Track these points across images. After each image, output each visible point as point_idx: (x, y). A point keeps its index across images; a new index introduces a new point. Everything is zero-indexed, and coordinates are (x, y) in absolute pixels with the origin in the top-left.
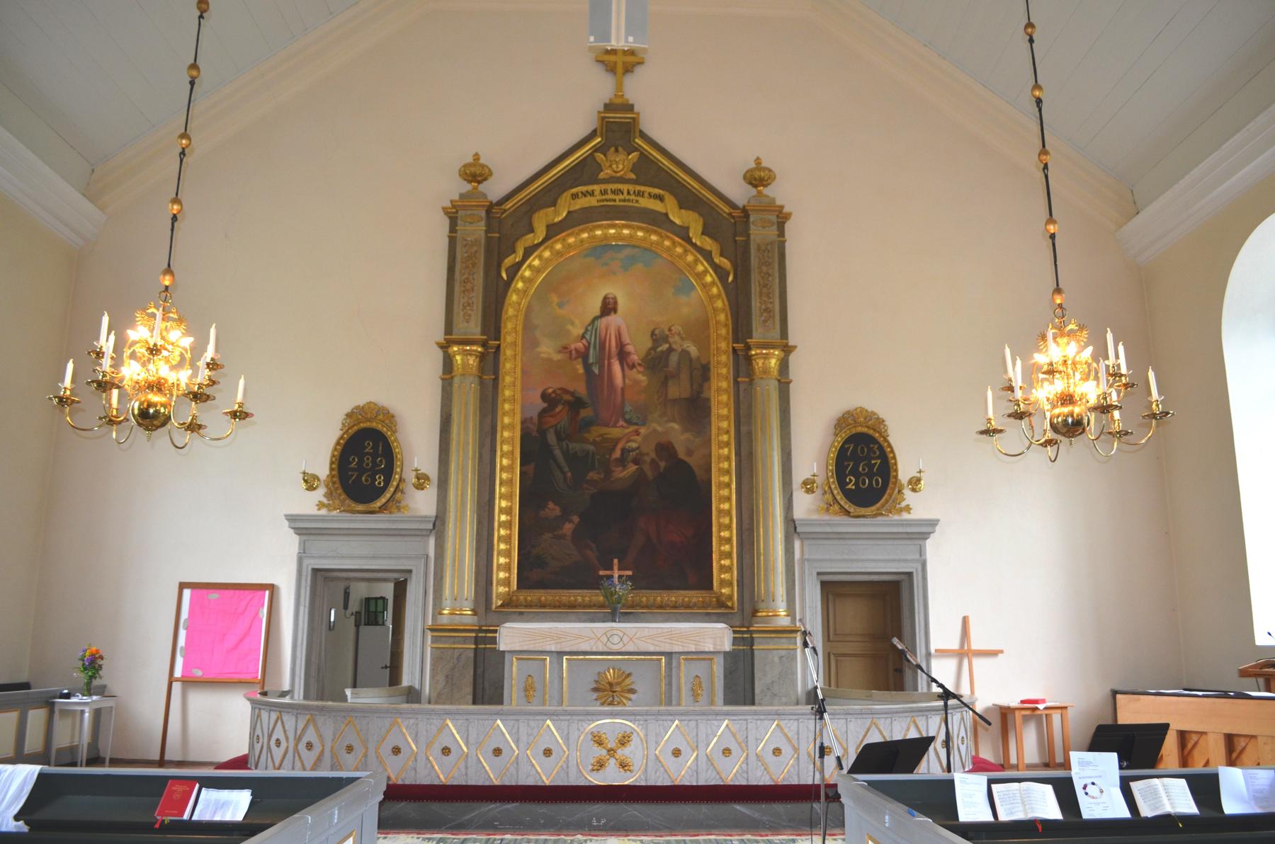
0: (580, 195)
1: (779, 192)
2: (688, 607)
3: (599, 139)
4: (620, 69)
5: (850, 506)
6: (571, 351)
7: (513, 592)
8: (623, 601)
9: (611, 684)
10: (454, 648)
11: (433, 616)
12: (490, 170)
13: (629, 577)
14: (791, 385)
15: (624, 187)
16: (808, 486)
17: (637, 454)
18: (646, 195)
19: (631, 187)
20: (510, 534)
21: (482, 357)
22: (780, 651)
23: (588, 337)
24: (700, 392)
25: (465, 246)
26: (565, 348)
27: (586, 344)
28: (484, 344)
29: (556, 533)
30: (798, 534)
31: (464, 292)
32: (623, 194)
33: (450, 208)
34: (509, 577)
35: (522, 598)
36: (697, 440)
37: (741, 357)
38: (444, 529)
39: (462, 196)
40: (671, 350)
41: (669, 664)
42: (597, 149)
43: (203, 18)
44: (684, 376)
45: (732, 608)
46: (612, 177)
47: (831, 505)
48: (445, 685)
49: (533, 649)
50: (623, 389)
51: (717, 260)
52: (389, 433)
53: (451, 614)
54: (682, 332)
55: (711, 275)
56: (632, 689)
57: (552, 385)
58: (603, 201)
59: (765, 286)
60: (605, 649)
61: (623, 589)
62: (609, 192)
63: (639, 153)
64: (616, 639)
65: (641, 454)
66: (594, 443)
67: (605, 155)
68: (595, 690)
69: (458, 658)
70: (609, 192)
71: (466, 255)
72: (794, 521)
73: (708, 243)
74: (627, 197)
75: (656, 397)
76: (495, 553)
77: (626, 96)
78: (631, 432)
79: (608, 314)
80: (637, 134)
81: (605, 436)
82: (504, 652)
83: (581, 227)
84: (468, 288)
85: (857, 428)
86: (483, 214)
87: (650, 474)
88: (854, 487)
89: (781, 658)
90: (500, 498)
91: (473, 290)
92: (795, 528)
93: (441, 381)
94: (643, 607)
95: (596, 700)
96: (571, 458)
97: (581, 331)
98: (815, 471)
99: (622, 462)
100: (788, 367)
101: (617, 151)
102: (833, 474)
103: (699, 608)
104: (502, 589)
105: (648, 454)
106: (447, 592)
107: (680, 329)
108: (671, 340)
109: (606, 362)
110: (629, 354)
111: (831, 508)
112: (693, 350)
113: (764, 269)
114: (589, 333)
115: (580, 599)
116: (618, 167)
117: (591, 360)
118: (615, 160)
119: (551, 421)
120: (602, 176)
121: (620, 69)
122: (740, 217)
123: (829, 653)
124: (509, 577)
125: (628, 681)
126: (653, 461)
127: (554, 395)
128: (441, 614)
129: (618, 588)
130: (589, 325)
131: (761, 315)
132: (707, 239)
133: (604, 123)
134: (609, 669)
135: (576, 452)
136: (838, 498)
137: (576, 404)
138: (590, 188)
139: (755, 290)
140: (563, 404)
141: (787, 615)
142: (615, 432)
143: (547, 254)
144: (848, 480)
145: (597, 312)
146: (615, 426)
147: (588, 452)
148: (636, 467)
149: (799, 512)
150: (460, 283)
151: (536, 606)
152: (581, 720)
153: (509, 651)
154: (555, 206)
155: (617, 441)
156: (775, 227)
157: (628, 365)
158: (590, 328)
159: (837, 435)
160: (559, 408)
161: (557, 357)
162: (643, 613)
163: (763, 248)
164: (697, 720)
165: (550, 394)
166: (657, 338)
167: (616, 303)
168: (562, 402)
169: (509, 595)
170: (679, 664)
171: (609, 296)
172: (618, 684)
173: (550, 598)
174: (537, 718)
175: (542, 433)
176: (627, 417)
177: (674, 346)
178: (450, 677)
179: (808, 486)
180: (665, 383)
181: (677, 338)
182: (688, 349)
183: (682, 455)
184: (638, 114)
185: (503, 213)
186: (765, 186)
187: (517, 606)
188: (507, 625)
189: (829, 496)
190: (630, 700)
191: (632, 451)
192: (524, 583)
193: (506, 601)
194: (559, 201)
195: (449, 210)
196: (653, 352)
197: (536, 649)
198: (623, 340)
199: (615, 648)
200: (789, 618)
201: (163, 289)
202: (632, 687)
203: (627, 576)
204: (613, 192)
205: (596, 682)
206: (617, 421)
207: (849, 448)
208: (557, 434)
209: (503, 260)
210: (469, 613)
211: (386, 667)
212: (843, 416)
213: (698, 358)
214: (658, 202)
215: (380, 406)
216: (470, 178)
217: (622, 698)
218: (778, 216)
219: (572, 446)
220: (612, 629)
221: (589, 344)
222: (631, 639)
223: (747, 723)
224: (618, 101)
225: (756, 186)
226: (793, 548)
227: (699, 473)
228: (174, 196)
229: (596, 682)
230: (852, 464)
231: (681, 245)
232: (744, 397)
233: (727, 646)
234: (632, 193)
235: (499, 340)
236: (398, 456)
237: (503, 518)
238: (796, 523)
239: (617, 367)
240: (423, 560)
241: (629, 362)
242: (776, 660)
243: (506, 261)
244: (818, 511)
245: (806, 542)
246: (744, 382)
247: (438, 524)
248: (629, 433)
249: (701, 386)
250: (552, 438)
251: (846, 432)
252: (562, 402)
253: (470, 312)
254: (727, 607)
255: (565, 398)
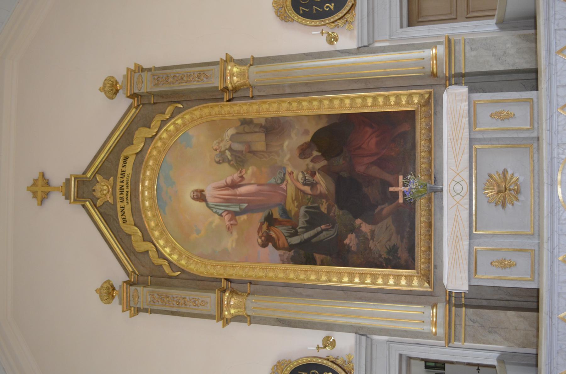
0: (123, 217)
1: (120, 74)
2: (429, 130)
3: (87, 203)
4: (46, 189)
5: (347, 6)
6: (231, 225)
7: (418, 273)
8: (425, 182)
9: (499, 192)
10: (465, 325)
11: (437, 340)
12: (105, 282)
13: (405, 177)
14: (255, 57)
15: (119, 185)
16: (332, 40)
17: (307, 173)
18: (124, 169)
19: (119, 180)
20: (370, 274)
21: (234, 292)
22: (466, 51)
23: (220, 212)
24: (261, 126)
25: (154, 302)
26: (229, 228)
27: (226, 213)
28: (224, 291)
29: (369, 238)
30: (369, 45)
31: (186, 305)
32: (123, 186)
33: (131, 312)
34: (405, 276)
35: (422, 266)
36: (296, 127)
37: (235, 95)
38: (365, 327)
39: (120, 304)
40: (230, 149)
41: (480, 141)
42: (95, 205)
44: (248, 138)
45: (430, 93)
46: (112, 194)
47: (347, 21)
48: (498, 334)
49: (467, 261)
50: (259, 185)
51: (168, 116)
52: (291, 366)
53: (436, 327)
54: (217, 141)
55: (177, 120)
56: (503, 173)
57: (256, 239)
58: (127, 200)
59: (182, 78)
60: (467, 197)
61: (413, 182)
62: (121, 196)
63: (97, 175)
64: (458, 187)
65: (307, 171)
66: (299, 207)
67: (98, 199)
68: (504, 205)
69: (474, 323)
70: (121, 196)
71: (160, 302)
72: (359, 48)
73: (156, 123)
74: (125, 183)
75: (265, 159)
76: (385, 287)
77: (62, 184)
78: (290, 178)
79: (205, 196)
80: (84, 176)
81: (294, 199)
82: (470, 286)
83: (143, 216)
84: (183, 302)
85: (288, 5)
86: (132, 288)
87: (324, 163)
88: (333, 4)
89: (472, 49)
90: (341, 282)
91: (184, 298)
92: (365, 46)
93: (252, 325)
94: (430, 167)
95: (513, 205)
96: (310, 225)
97: (217, 216)
98: (319, 32)
99: (313, 185)
100: (242, 60)
101: (94, 190)
102: (323, 21)
103: (430, 121)
104: (415, 282)
105: (307, 165)
106: (418, 328)
107: (215, 142)
108: (223, 149)
109: (239, 198)
110: (233, 181)
111: (348, 20)
112: (231, 132)
113: (170, 80)
114: (218, 211)
115: (423, 219)
116: (105, 190)
117: (237, 209)
118: (100, 191)
119: (282, 241)
120: (111, 201)
121: (46, 189)
122: (138, 100)
123: (467, 18)
124: (405, 276)
125: (496, 177)
126: (312, 161)
127: (263, 238)
128: (436, 334)
129: (412, 187)
130: (212, 210)
131: (202, 80)
132: (152, 125)
133: (78, 199)
134: (484, 194)
135: (306, 221)
136: (341, 15)
137: (270, 220)
138: (119, 210)
139: (184, 85)
140: (270, 231)
141: (436, 48)
142: (291, 192)
143: (162, 242)
144: (327, 9)
145: (203, 204)
146: (286, 191)
147: (306, 212)
148: (317, 173)
149: (353, 45)
150: (180, 307)
151: (429, 255)
152: (559, 219)
153: (469, 281)
154: (130, 236)
155: (297, 189)
156: (143, 74)
157: (240, 181)
158: (214, 210)
159: (293, 20)
160: (272, 233)
161: (235, 235)
162: (435, 167)
163: (156, 82)
164: (558, 87)
165: (262, 241)
166: (222, 160)
167: (197, 191)
168: (268, 231)
169: (420, 276)
170: (480, 131)
171: (192, 195)
172: (498, 186)
173: (423, 243)
174: (556, 272)
175: (291, 247)
176: (279, 181)
177: (228, 146)
178: (490, 329)
179: (332, 40)
180: (254, 153)
181: (222, 144)
182: (230, 136)
183: (308, 138)
184: (71, 175)
185: (135, 273)
186: (117, 83)
187: (429, 271)
188: (445, 282)
189: (340, 23)
190: (513, 174)
191: (305, 177)
192: (410, 264)
193: (425, 279)
194: (127, 232)
195: (133, 312)
196: (232, 162)
197: (467, 257)
198: (223, 185)
199: (466, 187)
200: (438, 46)
202: (501, 173)
203: (403, 179)
204: (122, 193)
205: (496, 205)
206: (282, 189)
207: (303, 10)
208: (292, 235)
209: (167, 274)
210: (435, 310)
211: (478, 369)
212: (279, 16)
213: (237, 128)
214: (128, 161)
215: (271, 371)
216: (111, 296)
217: (512, 181)
218: (135, 73)
219: (301, 225)
220: (449, 191)
221: (226, 210)
222: (458, 174)
223: (559, 30)
224: (64, 190)
225: (117, 91)
226: (380, 47)
227: (322, 124)
229: (496, 205)
230: (314, 7)
231: (156, 142)
232: (264, 91)
233: (464, 90)
234: (122, 180)
235: (221, 279)
236: (309, 360)
237: (357, 280)
238: (360, 46)
239: (242, 190)
240: (391, 345)
241: (238, 181)
242: (473, 53)
243: (167, 272)
244: (351, 30)
245: (376, 38)
246: (252, 92)
247: (360, 331)
248: (292, 181)
249: (256, 125)
250: (295, 240)
251: (290, 14)
252: (268, 231)
253: (200, 301)
254: (429, 98)
255: (265, 230)
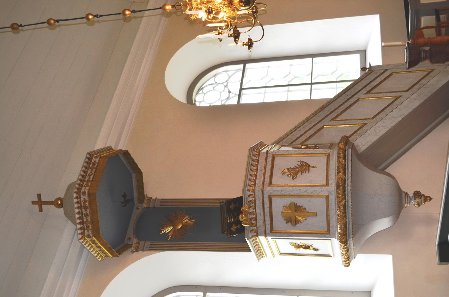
43: (21, 25)
201: (174, 8)
228: (121, 15)
